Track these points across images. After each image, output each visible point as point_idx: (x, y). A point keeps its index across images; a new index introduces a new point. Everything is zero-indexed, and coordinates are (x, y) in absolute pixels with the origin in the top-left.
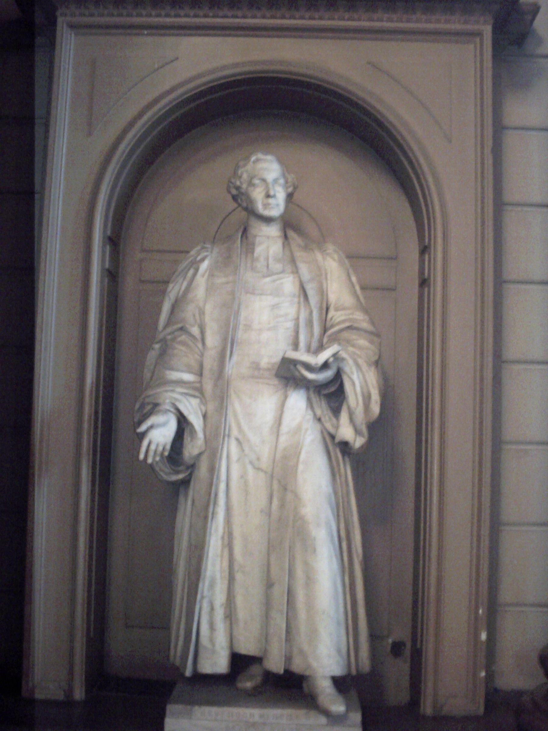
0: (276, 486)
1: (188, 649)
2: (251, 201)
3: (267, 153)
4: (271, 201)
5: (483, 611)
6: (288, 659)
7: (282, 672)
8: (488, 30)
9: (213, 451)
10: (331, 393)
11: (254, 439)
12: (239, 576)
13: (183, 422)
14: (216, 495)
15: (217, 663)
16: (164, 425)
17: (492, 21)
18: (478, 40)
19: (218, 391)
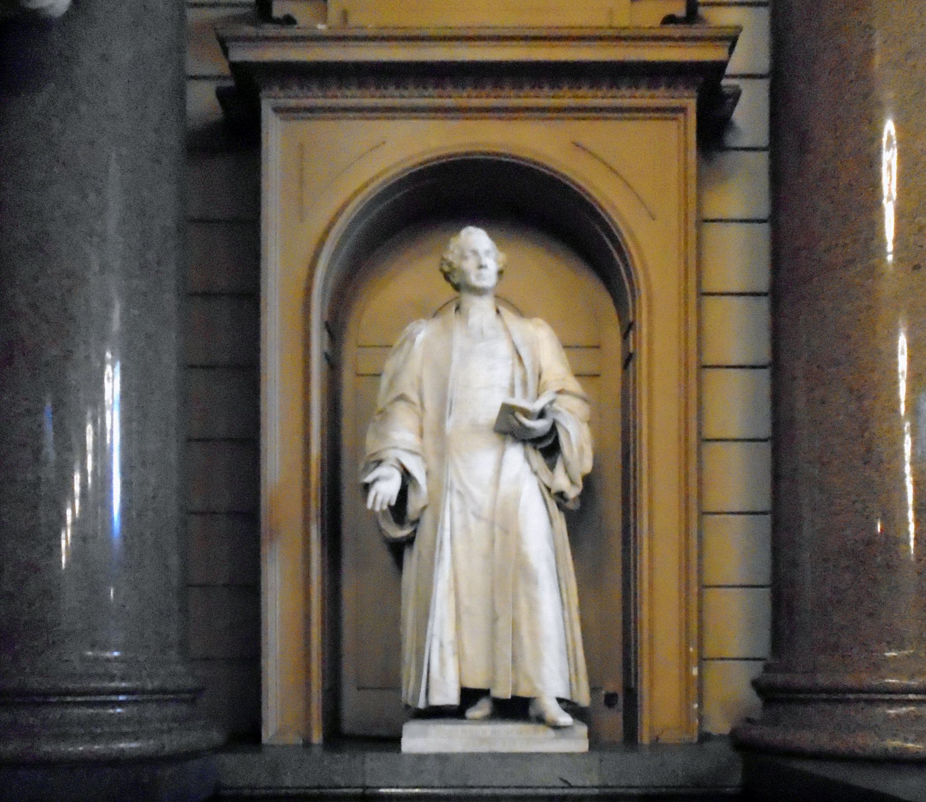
0: (497, 530)
2: (463, 273)
3: (478, 226)
4: (483, 271)
6: (515, 686)
7: (509, 697)
8: (691, 104)
9: (435, 504)
10: (548, 447)
11: (477, 493)
12: (465, 618)
13: (406, 475)
14: (441, 542)
15: (448, 695)
16: (387, 478)
17: (695, 94)
18: (681, 116)
19: (440, 446)
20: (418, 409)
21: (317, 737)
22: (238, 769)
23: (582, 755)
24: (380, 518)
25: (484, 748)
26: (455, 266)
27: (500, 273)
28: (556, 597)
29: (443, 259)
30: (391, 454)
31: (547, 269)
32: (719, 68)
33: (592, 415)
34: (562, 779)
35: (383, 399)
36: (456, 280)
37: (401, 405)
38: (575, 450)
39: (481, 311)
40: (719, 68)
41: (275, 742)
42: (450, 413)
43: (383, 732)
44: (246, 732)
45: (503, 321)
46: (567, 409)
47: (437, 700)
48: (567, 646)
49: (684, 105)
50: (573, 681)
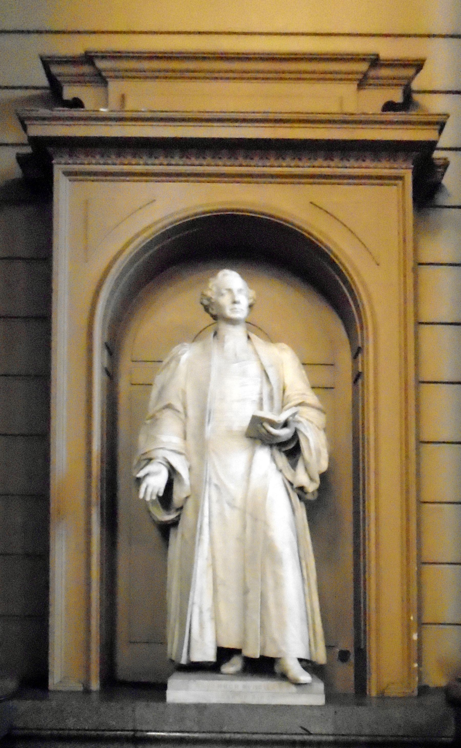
1: (183, 641)
2: (220, 307)
3: (232, 268)
4: (236, 306)
5: (414, 618)
6: (263, 648)
7: (258, 656)
9: (196, 495)
10: (291, 450)
11: (231, 487)
12: (221, 589)
13: (172, 471)
14: (201, 526)
15: (205, 653)
16: (156, 473)
18: (400, 182)
19: (201, 449)
20: (183, 416)
21: (95, 685)
22: (27, 713)
23: (319, 707)
24: (150, 505)
25: (237, 700)
26: (213, 301)
27: (251, 306)
28: (297, 573)
29: (203, 295)
30: (160, 454)
31: (288, 299)
32: (432, 146)
33: (327, 422)
34: (302, 728)
35: (153, 406)
36: (214, 312)
37: (168, 413)
38: (314, 452)
39: (235, 337)
40: (432, 146)
41: (60, 688)
42: (209, 421)
43: (151, 679)
44: (36, 679)
45: (253, 345)
46: (307, 420)
47: (197, 657)
48: (307, 612)
49: (402, 175)
50: (312, 640)
